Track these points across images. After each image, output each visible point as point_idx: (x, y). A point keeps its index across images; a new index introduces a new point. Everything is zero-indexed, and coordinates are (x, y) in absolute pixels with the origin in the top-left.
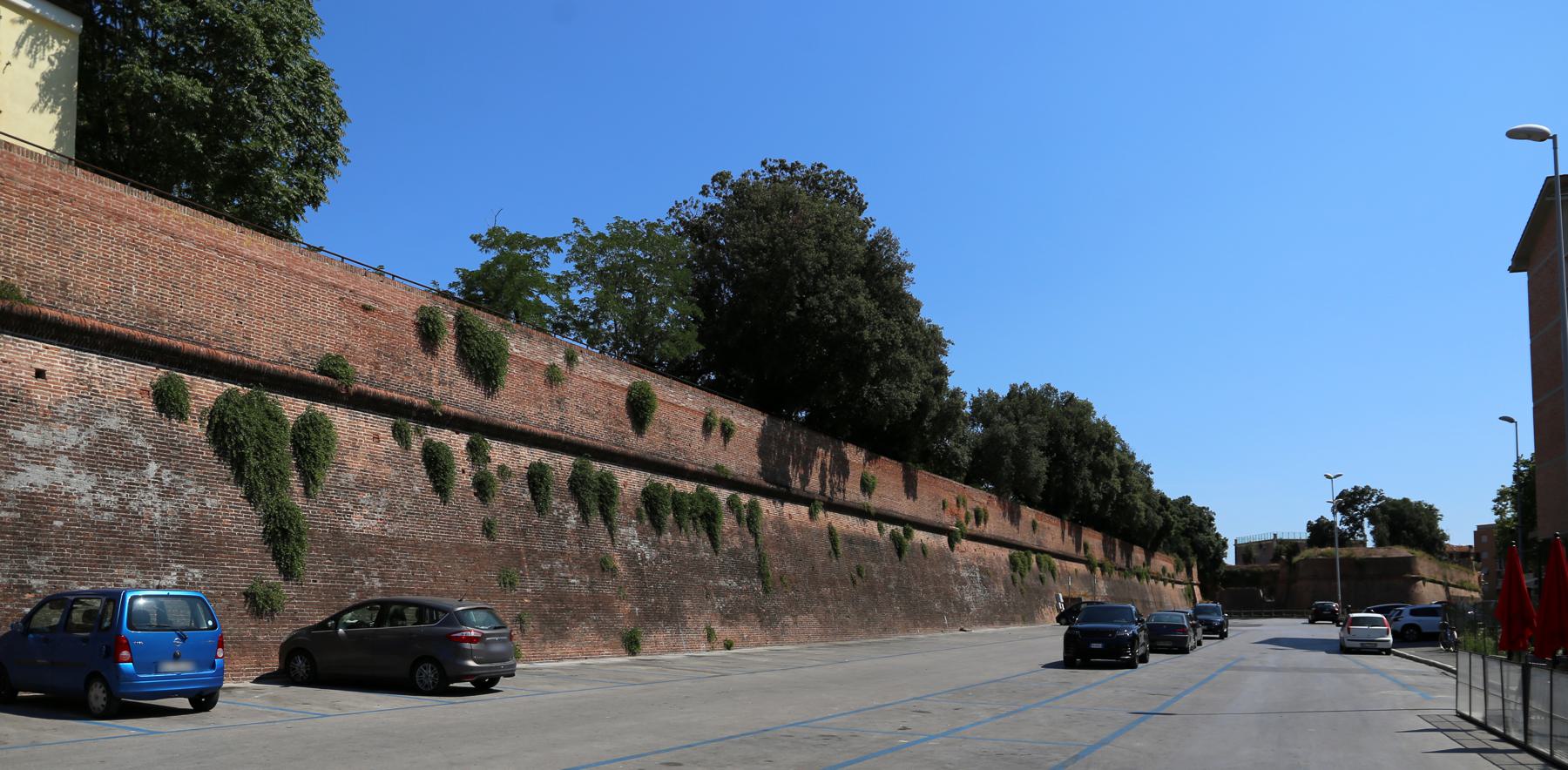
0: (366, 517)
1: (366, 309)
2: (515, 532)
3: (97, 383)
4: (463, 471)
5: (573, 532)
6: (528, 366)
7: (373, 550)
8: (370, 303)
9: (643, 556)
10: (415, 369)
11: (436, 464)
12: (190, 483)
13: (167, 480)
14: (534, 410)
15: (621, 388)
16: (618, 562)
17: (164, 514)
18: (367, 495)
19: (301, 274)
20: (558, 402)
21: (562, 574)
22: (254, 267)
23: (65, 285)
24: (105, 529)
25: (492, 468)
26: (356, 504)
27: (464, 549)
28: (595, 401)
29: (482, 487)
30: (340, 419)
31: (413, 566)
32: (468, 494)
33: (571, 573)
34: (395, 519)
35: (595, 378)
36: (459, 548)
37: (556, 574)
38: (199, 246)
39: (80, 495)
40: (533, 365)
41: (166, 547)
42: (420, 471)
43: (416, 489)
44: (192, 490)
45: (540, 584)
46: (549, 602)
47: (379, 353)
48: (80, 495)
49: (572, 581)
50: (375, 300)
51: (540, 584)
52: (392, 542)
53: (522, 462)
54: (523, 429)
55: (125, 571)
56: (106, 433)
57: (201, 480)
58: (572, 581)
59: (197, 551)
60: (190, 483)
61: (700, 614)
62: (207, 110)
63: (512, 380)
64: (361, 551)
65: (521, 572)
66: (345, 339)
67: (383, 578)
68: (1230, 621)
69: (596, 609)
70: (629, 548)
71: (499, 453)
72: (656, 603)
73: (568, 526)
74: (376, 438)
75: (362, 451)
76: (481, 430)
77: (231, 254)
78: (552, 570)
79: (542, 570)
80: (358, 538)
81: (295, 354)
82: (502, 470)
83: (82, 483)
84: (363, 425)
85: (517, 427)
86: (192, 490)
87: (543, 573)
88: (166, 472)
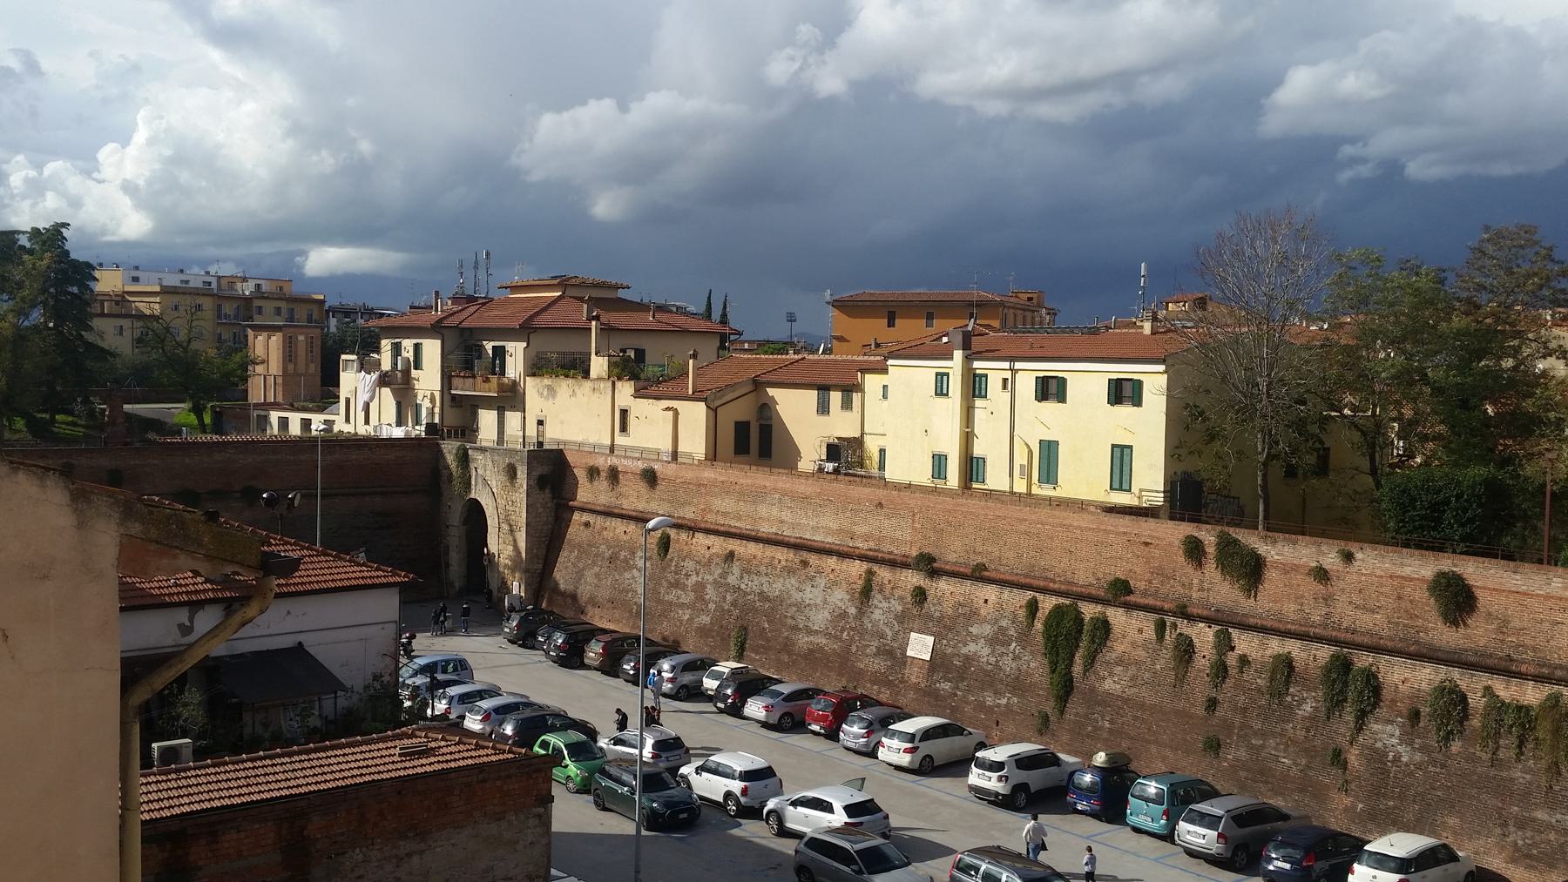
0: (1114, 682)
1: (1147, 544)
2: (1235, 709)
3: (1004, 604)
4: (1204, 657)
5: (1304, 718)
6: (1288, 569)
7: (1112, 703)
8: (1149, 541)
9: (1397, 758)
10: (1179, 582)
11: (1186, 650)
12: (1026, 654)
13: (1017, 652)
14: (1293, 607)
15: (1422, 580)
16: (1353, 758)
17: (1011, 668)
18: (1120, 668)
19: (1105, 530)
20: (1324, 599)
21: (1273, 752)
22: (1079, 532)
23: (1000, 558)
24: (987, 673)
25: (1231, 660)
26: (1111, 674)
27: (1183, 715)
28: (1378, 596)
29: (1220, 671)
30: (1116, 616)
31: (1136, 718)
32: (1201, 674)
33: (1285, 752)
34: (1134, 686)
35: (1379, 573)
36: (1177, 713)
37: (1267, 751)
38: (1053, 526)
39: (983, 657)
40: (1295, 568)
41: (1007, 685)
42: (1167, 654)
43: (1158, 667)
44: (1026, 658)
45: (1243, 754)
46: (1248, 771)
47: (1152, 573)
48: (983, 657)
49: (1283, 760)
50: (1153, 537)
51: (1243, 754)
52: (1126, 701)
53: (1269, 652)
54: (170, 666)
55: (988, 694)
56: (1001, 628)
57: (1032, 652)
58: (1283, 760)
59: (1020, 689)
60: (1026, 654)
61: (1471, 838)
62: (46, 323)
63: (1272, 580)
64: (1104, 703)
65: (1228, 741)
66: (1129, 566)
67: (1112, 722)
68: (890, 362)
69: (1302, 790)
70: (1379, 745)
71: (1244, 643)
72: (1395, 807)
73: (1300, 712)
74: (1140, 631)
75: (1129, 639)
76: (1225, 622)
77: (1068, 527)
78: (1263, 746)
79: (1252, 744)
80: (1105, 695)
81: (1098, 579)
82: (1244, 660)
83: (986, 651)
84: (1134, 622)
85: (1257, 623)
86: (1026, 658)
87: (1251, 747)
88: (1019, 647)
